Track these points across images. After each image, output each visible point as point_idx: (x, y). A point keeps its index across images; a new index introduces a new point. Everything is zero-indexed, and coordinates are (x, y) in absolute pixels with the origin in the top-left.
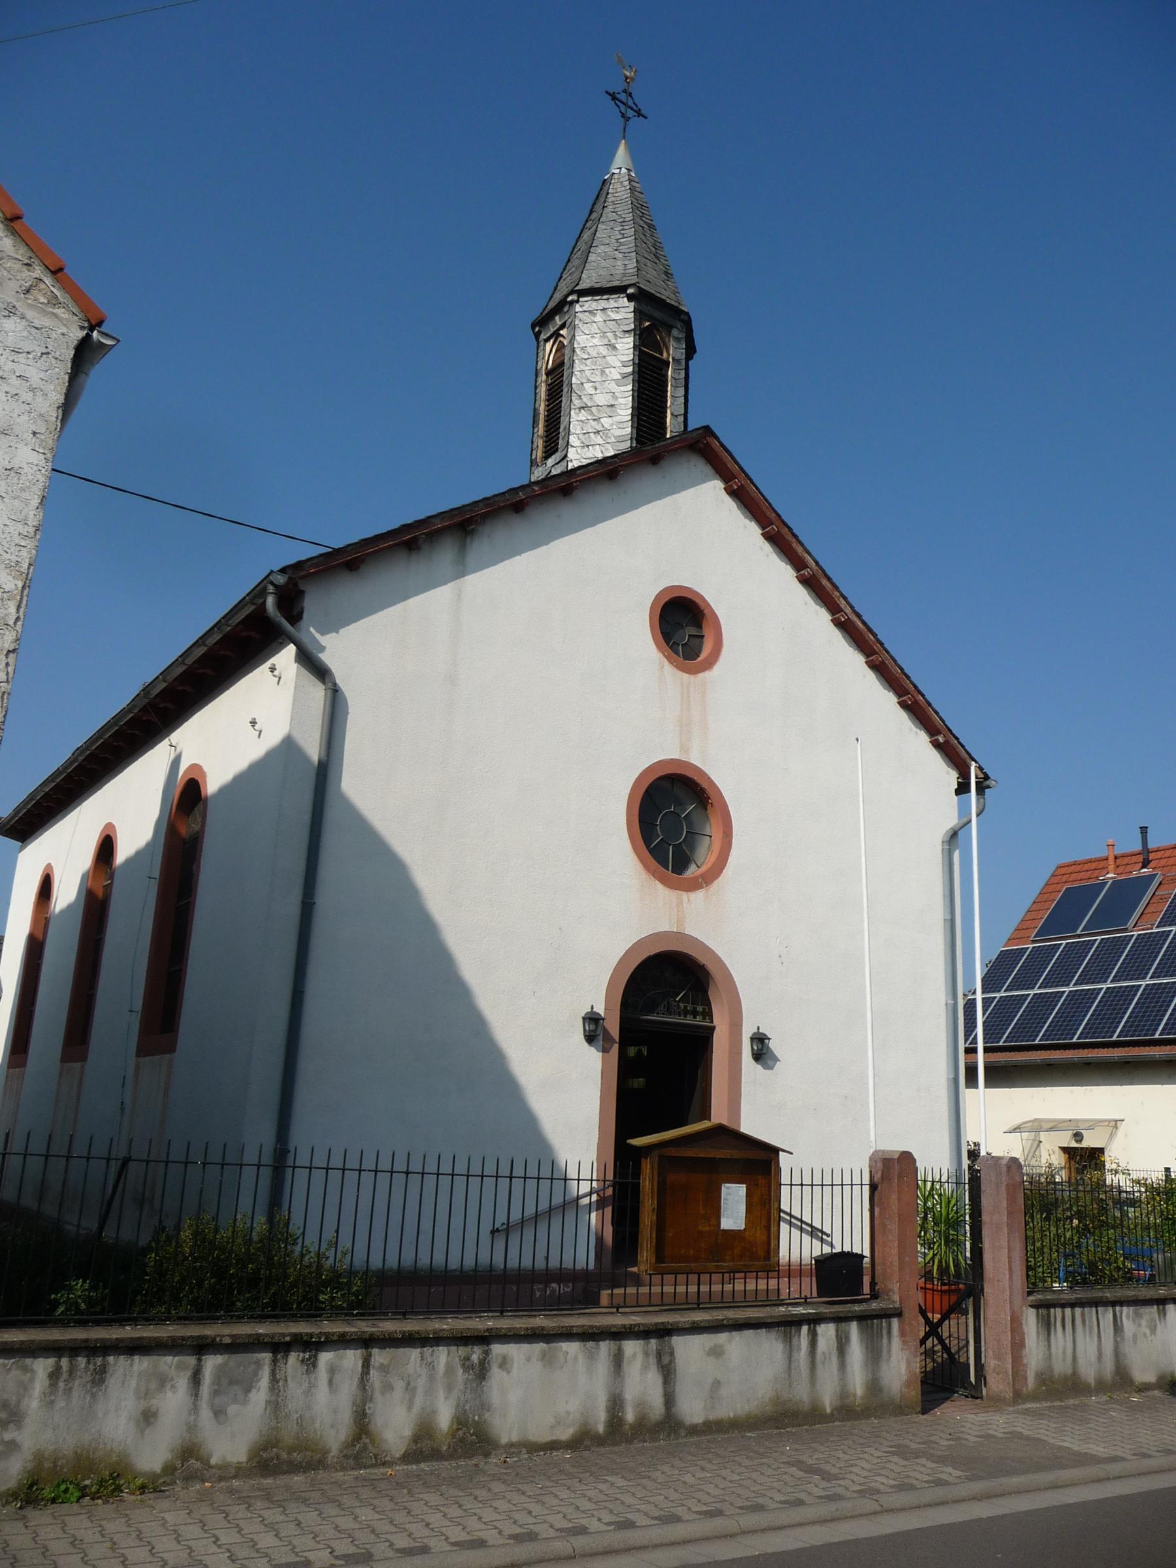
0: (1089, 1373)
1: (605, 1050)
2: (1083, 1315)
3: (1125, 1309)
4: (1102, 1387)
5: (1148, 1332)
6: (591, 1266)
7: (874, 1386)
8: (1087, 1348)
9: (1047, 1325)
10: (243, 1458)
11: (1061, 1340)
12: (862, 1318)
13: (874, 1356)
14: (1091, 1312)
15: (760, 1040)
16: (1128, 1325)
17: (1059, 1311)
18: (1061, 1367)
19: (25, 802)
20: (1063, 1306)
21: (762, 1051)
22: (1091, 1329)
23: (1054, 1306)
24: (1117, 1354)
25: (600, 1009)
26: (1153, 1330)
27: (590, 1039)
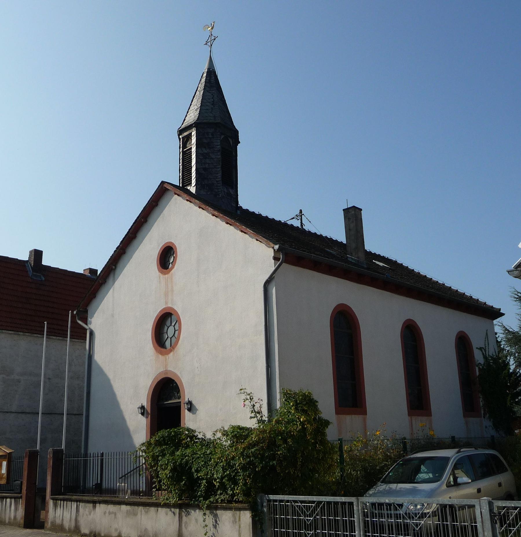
0: (66, 525)
1: (147, 418)
2: (67, 504)
3: (81, 504)
4: (70, 531)
5: (88, 513)
6: (144, 489)
7: (15, 517)
8: (67, 515)
9: (55, 506)
10: (82, 532)
11: (59, 511)
12: (15, 498)
13: (16, 509)
14: (69, 503)
15: (190, 403)
16: (81, 510)
17: (59, 502)
18: (58, 521)
19: (480, 318)
20: (61, 500)
21: (191, 407)
22: (69, 509)
23: (58, 500)
24: (76, 520)
25: (145, 404)
26: (90, 514)
27: (143, 414)
